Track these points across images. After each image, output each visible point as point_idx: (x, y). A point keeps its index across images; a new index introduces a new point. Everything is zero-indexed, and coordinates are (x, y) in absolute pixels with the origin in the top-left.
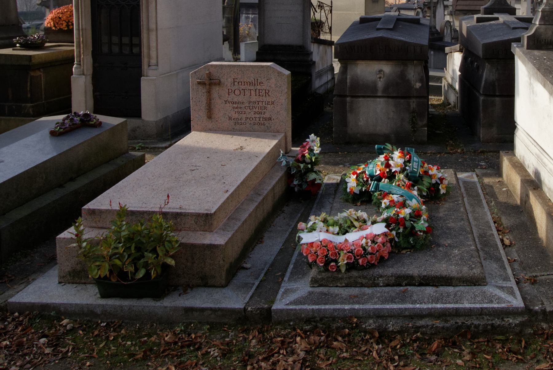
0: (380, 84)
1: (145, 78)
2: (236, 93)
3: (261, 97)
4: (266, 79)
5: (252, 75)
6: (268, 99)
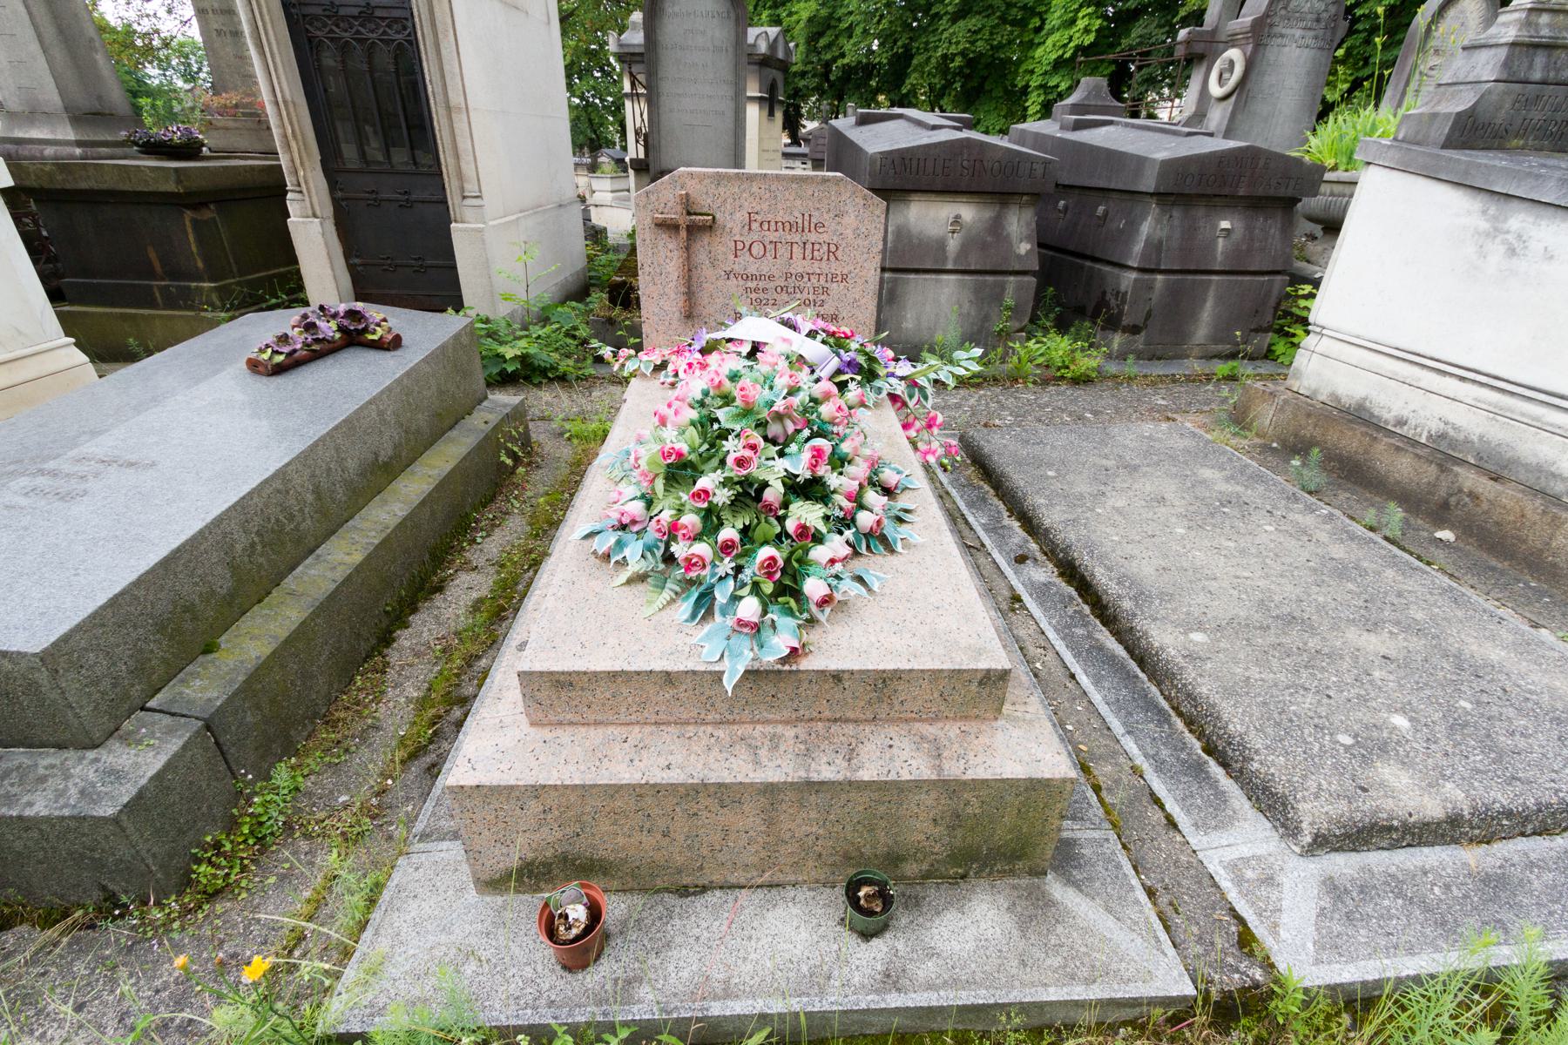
0: (953, 244)
2: (754, 251)
3: (817, 264)
5: (798, 202)
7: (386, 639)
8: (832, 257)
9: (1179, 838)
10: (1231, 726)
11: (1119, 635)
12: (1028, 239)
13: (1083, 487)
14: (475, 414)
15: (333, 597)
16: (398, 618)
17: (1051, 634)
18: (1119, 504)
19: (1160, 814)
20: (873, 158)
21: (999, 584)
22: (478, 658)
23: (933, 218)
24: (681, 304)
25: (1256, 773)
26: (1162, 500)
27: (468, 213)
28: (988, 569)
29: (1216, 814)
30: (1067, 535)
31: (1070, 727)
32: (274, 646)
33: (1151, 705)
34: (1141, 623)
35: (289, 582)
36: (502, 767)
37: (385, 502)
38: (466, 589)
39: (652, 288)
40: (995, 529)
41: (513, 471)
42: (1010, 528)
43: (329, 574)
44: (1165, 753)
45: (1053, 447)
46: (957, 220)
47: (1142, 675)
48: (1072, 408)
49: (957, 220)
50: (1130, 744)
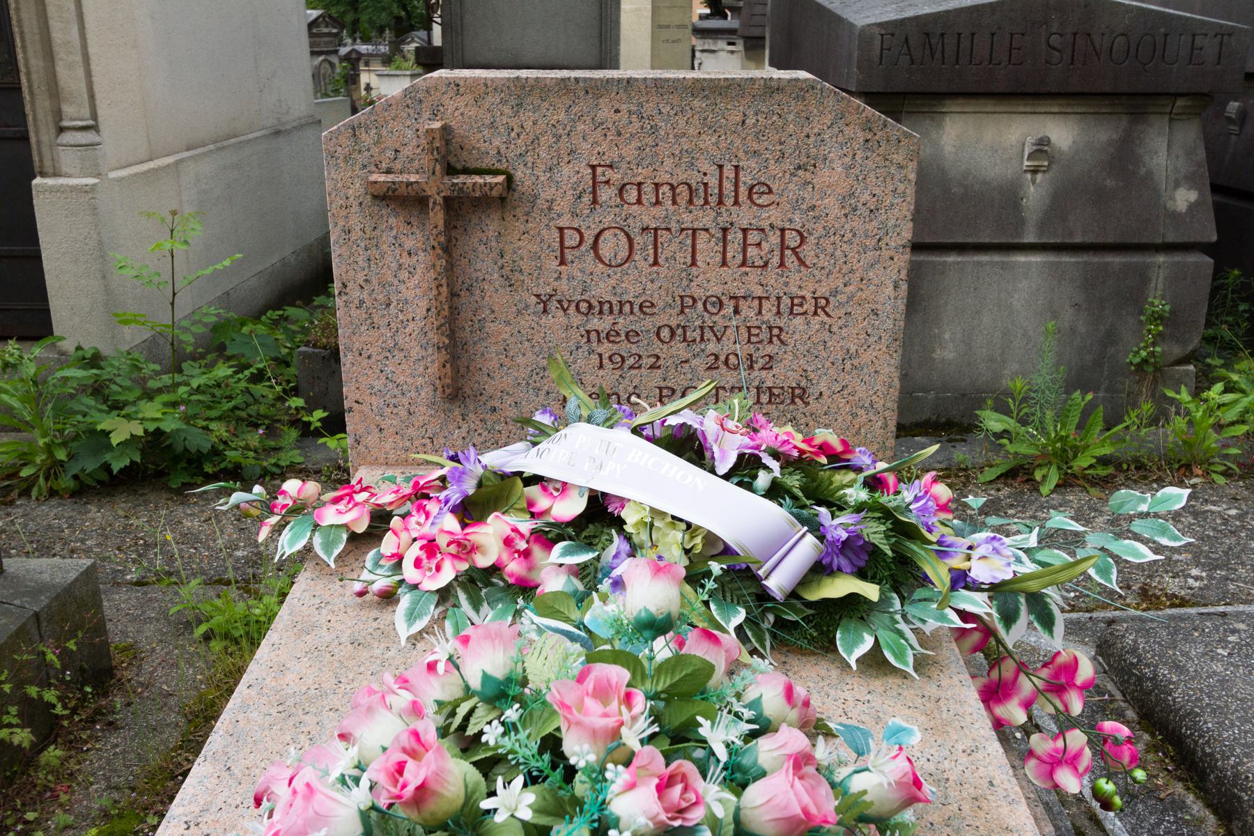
0: (1035, 194)
1: (50, 181)
2: (606, 250)
3: (754, 275)
4: (788, 165)
5: (708, 141)
6: (797, 282)
8: (790, 259)
12: (1191, 180)
20: (865, 35)
23: (994, 144)
24: (434, 369)
27: (67, 159)
39: (366, 335)
41: (28, 758)
46: (1042, 148)
49: (1042, 148)
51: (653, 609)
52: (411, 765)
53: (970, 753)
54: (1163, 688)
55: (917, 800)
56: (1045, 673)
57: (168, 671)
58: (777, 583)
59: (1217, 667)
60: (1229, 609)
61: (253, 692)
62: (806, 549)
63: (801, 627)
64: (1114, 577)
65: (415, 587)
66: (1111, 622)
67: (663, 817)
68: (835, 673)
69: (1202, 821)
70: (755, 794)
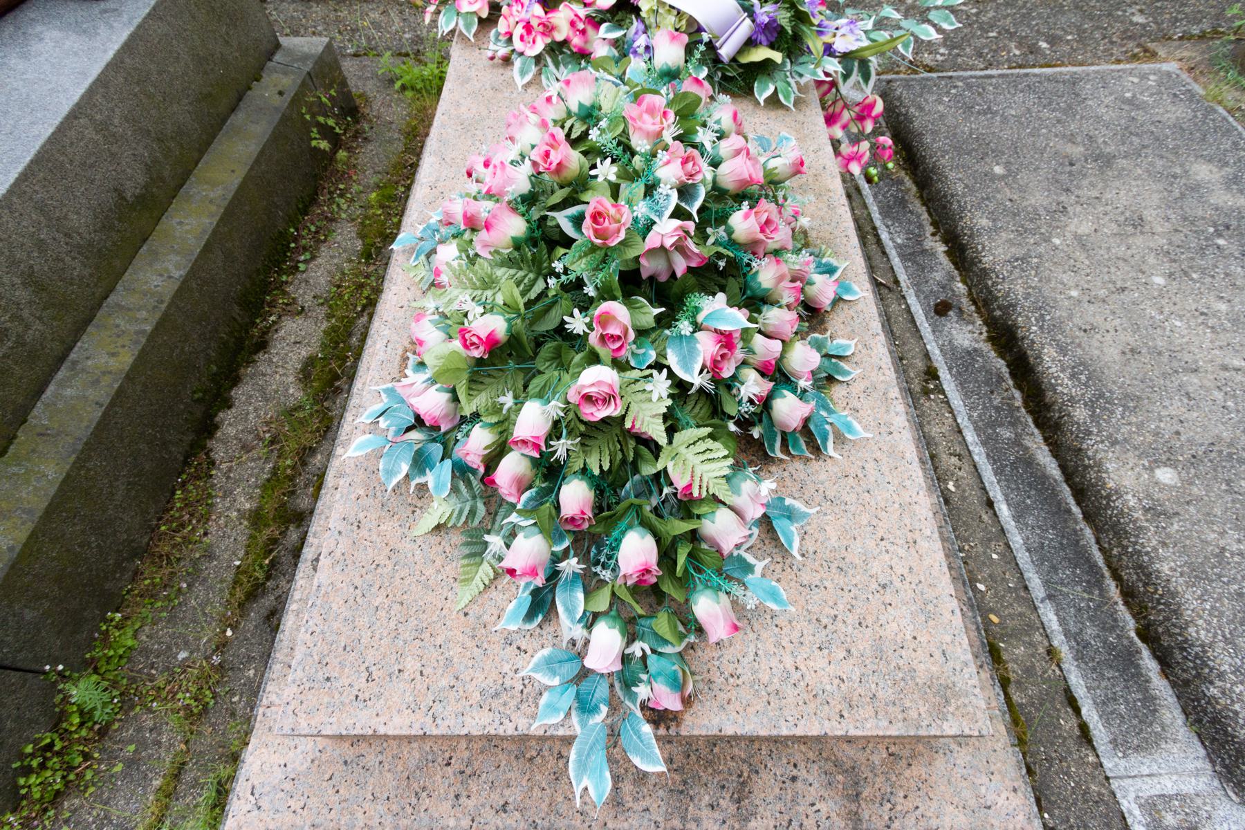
7: (208, 428)
9: (1091, 759)
10: (1192, 630)
11: (1056, 449)
13: (1038, 199)
14: (266, 78)
15: (103, 425)
16: (218, 395)
17: (970, 436)
18: (1085, 228)
19: (1074, 722)
21: (913, 348)
22: (313, 451)
25: (1211, 700)
26: (1138, 223)
28: (900, 324)
29: (1140, 733)
30: (1014, 288)
31: (981, 587)
32: (30, 526)
33: (1081, 558)
34: (1095, 447)
35: (39, 415)
36: (295, 805)
37: (155, 254)
38: (296, 339)
40: (915, 255)
41: (331, 157)
42: (933, 254)
43: (92, 394)
44: (1090, 631)
45: (1005, 120)
47: (1076, 509)
48: (1024, 31)
50: (1049, 616)
51: (670, 64)
52: (552, 153)
53: (815, 152)
54: (909, 119)
55: (800, 172)
56: (857, 109)
57: (389, 111)
58: (726, 52)
59: (941, 108)
60: (955, 74)
61: (446, 117)
62: (745, 28)
63: (738, 78)
64: (911, 50)
65: (522, 54)
66: (889, 82)
67: (684, 178)
68: (751, 107)
69: (909, 190)
70: (724, 169)
